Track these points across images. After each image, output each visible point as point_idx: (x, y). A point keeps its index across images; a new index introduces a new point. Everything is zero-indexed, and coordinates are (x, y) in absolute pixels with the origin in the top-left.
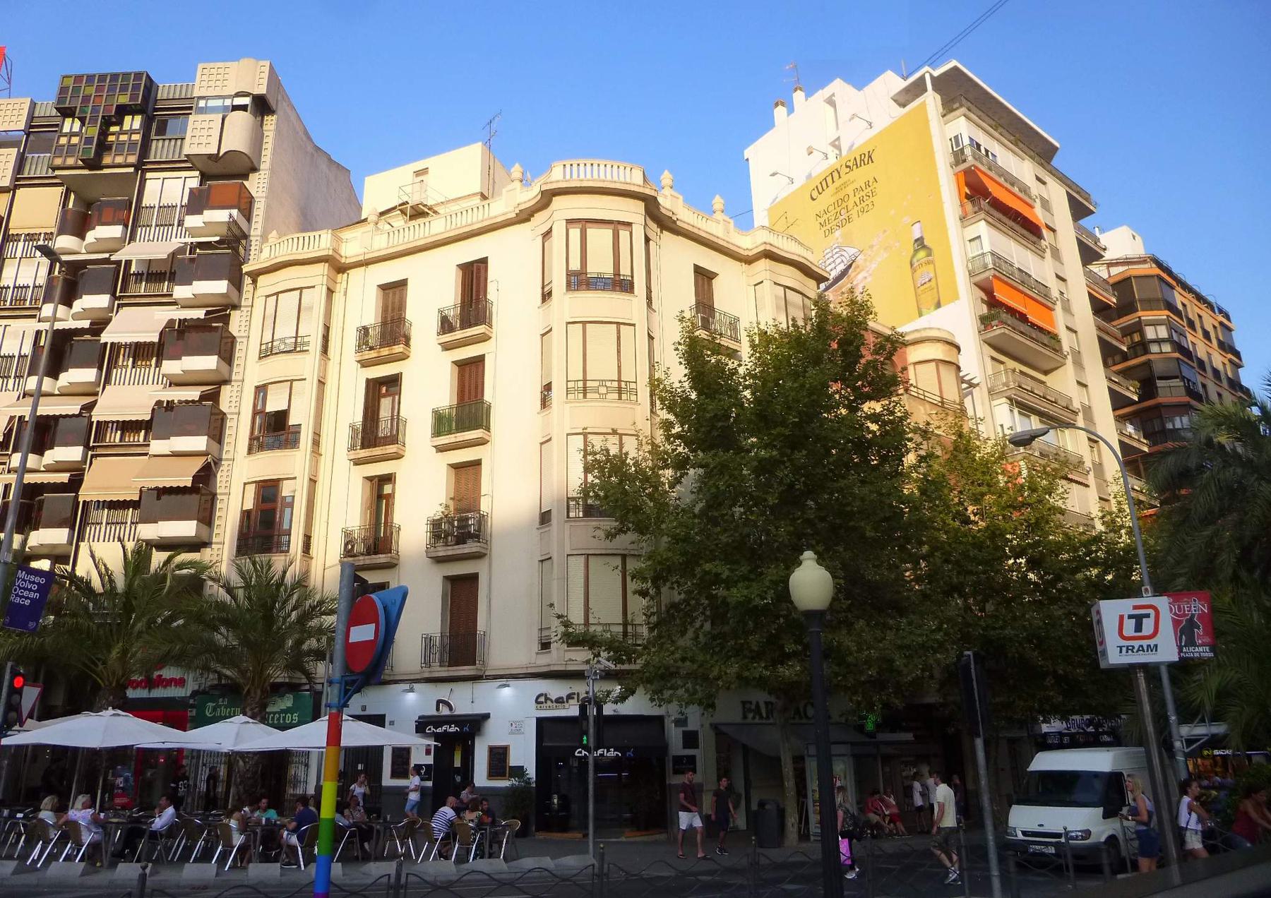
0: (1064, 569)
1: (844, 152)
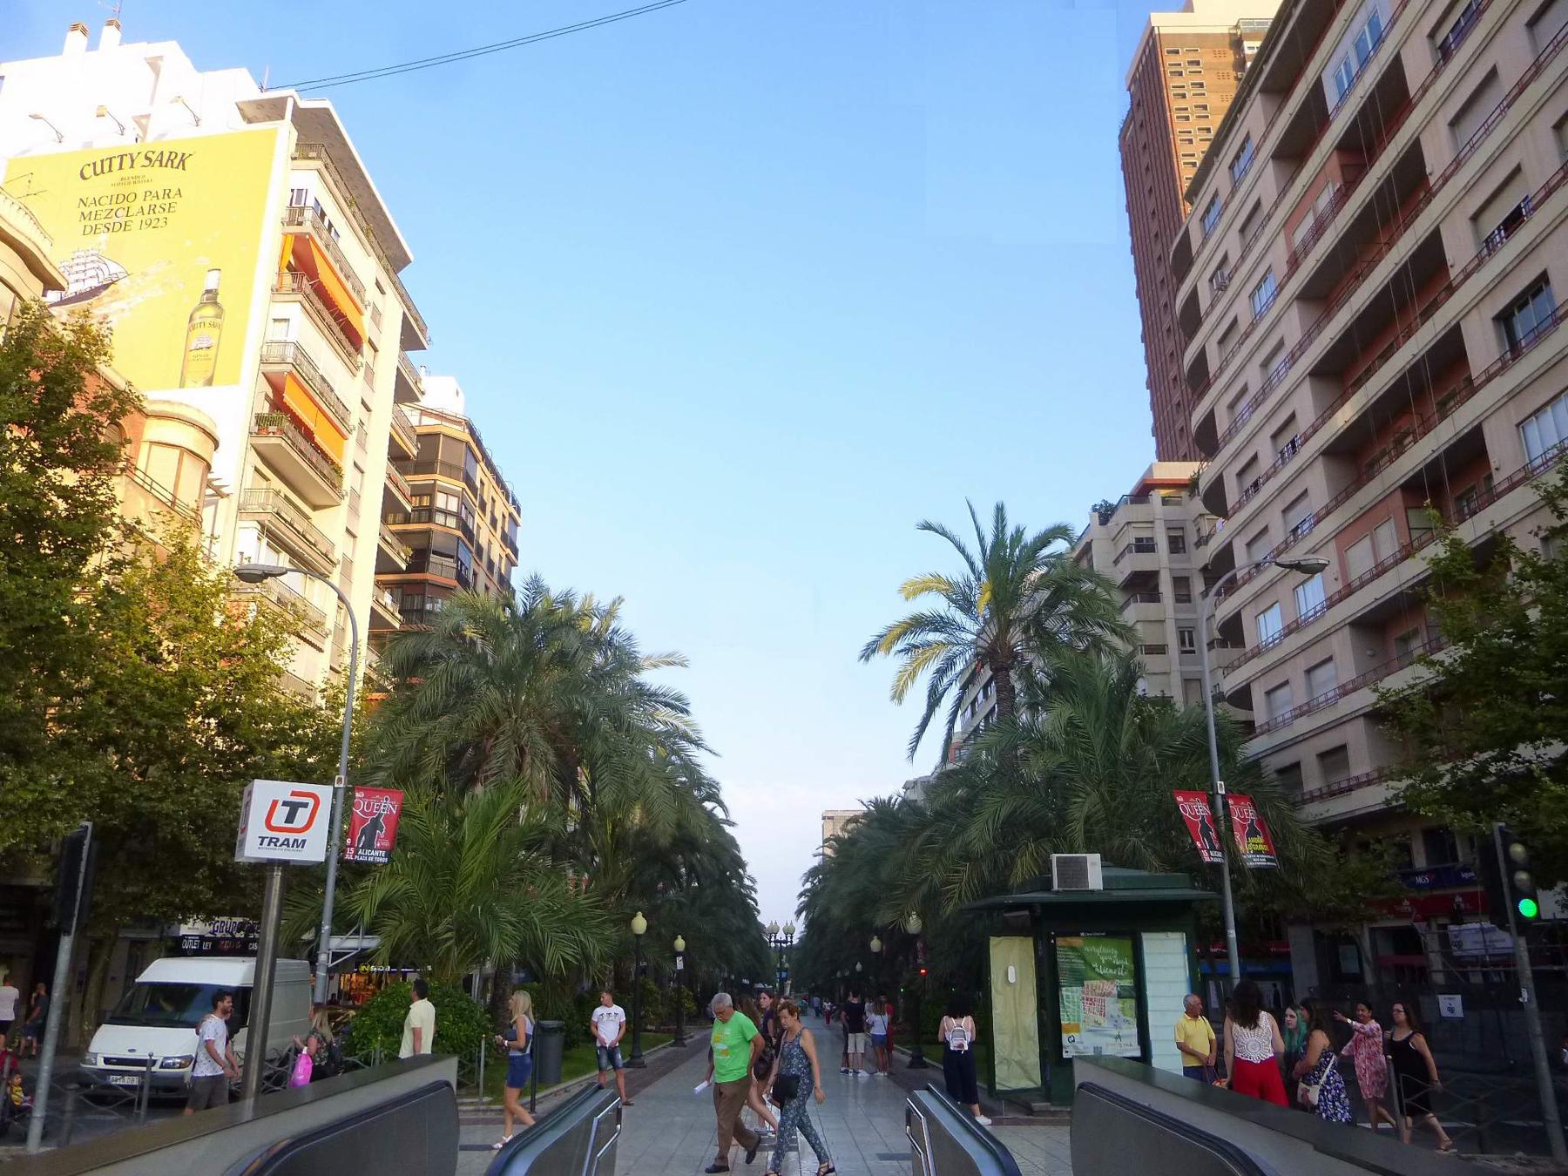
0: (260, 742)
1: (150, 138)
